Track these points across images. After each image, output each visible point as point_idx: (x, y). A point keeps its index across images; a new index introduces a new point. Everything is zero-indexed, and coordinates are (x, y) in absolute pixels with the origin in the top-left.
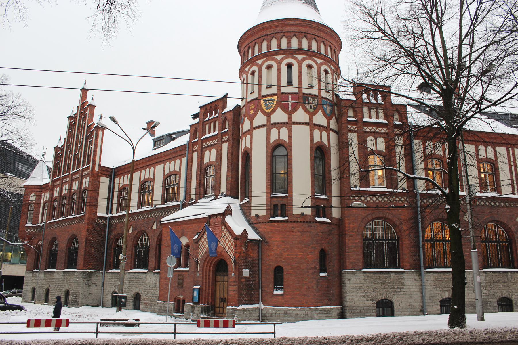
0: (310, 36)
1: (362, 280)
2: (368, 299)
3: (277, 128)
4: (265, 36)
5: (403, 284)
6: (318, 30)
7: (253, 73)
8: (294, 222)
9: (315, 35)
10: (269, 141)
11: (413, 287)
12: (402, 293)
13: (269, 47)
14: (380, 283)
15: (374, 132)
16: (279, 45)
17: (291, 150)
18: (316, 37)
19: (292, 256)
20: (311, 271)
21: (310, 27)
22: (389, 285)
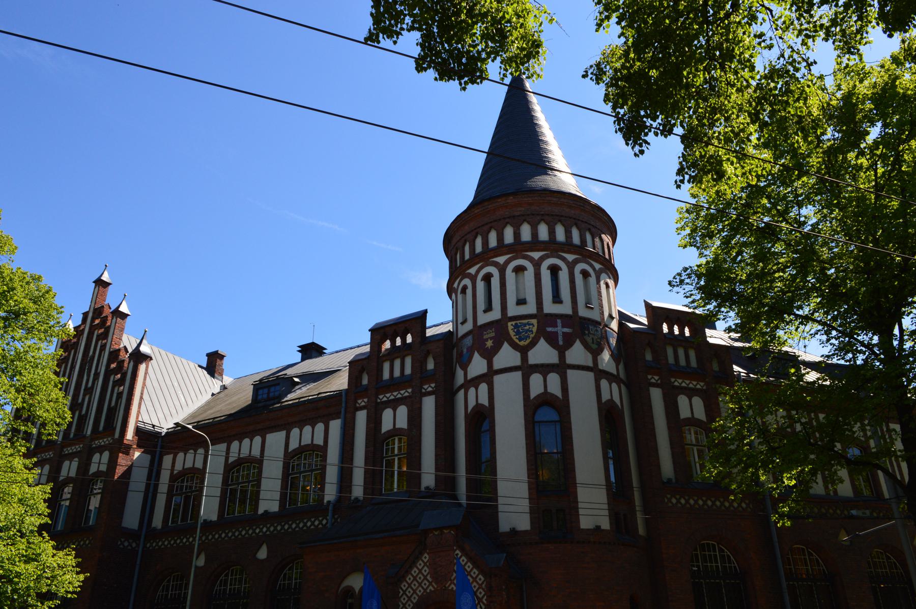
3: (540, 373)
9: (590, 224)
10: (529, 396)
13: (485, 243)
16: (535, 234)
17: (569, 413)
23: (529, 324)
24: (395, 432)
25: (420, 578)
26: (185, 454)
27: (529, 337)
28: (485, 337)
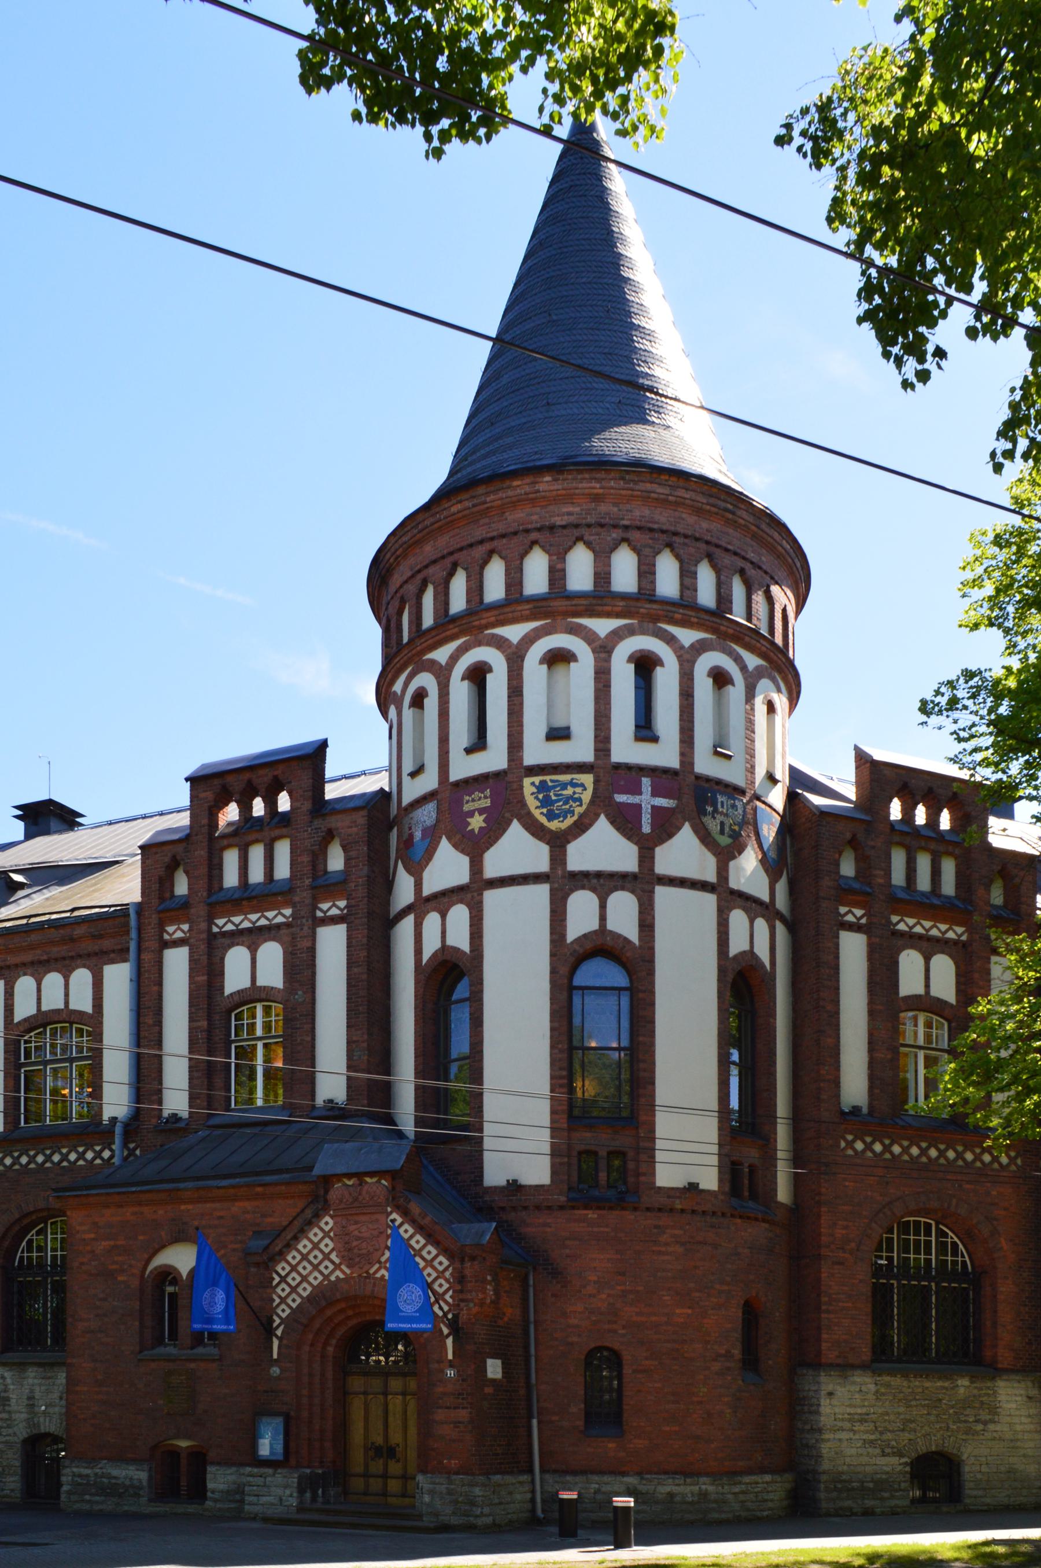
0: (727, 560)
1: (870, 1396)
2: (888, 1450)
3: (593, 890)
4: (539, 530)
5: (994, 1410)
6: (754, 537)
7: (419, 699)
8: (660, 1210)
9: (744, 558)
10: (563, 936)
11: (1024, 1420)
12: (988, 1435)
13: (476, 589)
14: (924, 1406)
15: (920, 937)
18: (748, 566)
19: (654, 1319)
20: (716, 1366)
21: (728, 522)
22: (951, 1411)
23: (574, 785)
24: (255, 995)
25: (283, 1290)
26: (443, 917)
27: (573, 812)
28: (466, 808)
